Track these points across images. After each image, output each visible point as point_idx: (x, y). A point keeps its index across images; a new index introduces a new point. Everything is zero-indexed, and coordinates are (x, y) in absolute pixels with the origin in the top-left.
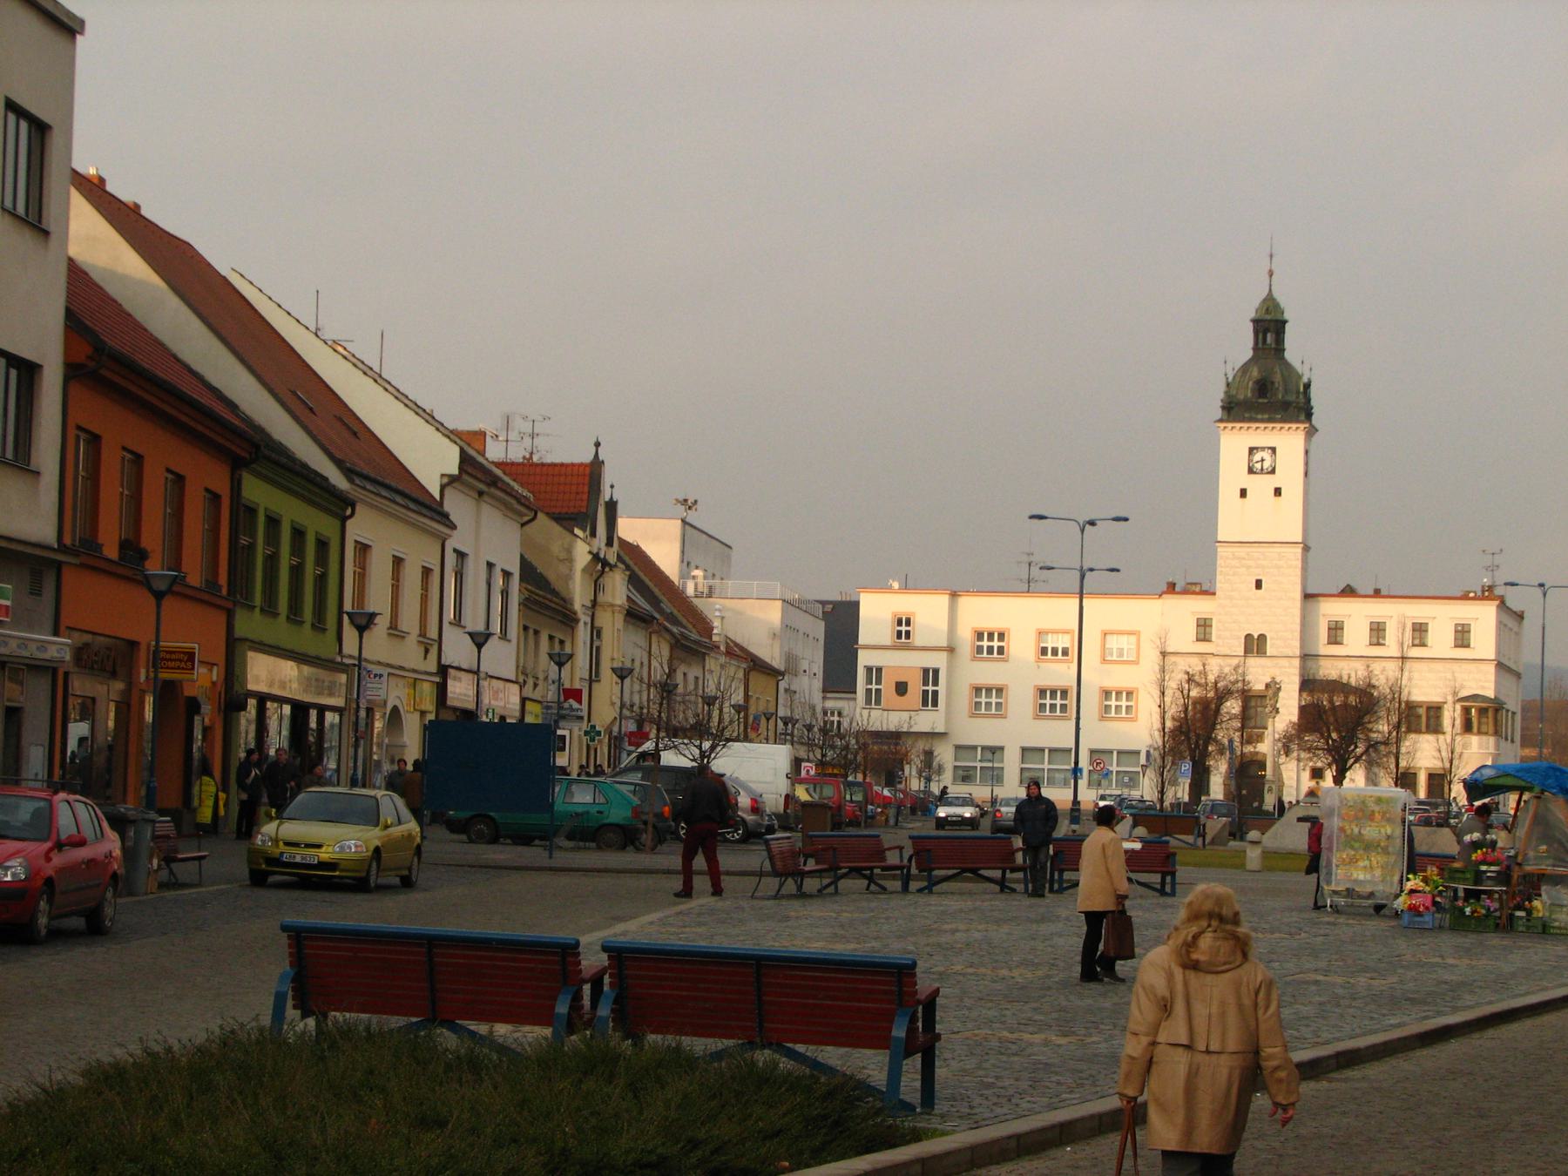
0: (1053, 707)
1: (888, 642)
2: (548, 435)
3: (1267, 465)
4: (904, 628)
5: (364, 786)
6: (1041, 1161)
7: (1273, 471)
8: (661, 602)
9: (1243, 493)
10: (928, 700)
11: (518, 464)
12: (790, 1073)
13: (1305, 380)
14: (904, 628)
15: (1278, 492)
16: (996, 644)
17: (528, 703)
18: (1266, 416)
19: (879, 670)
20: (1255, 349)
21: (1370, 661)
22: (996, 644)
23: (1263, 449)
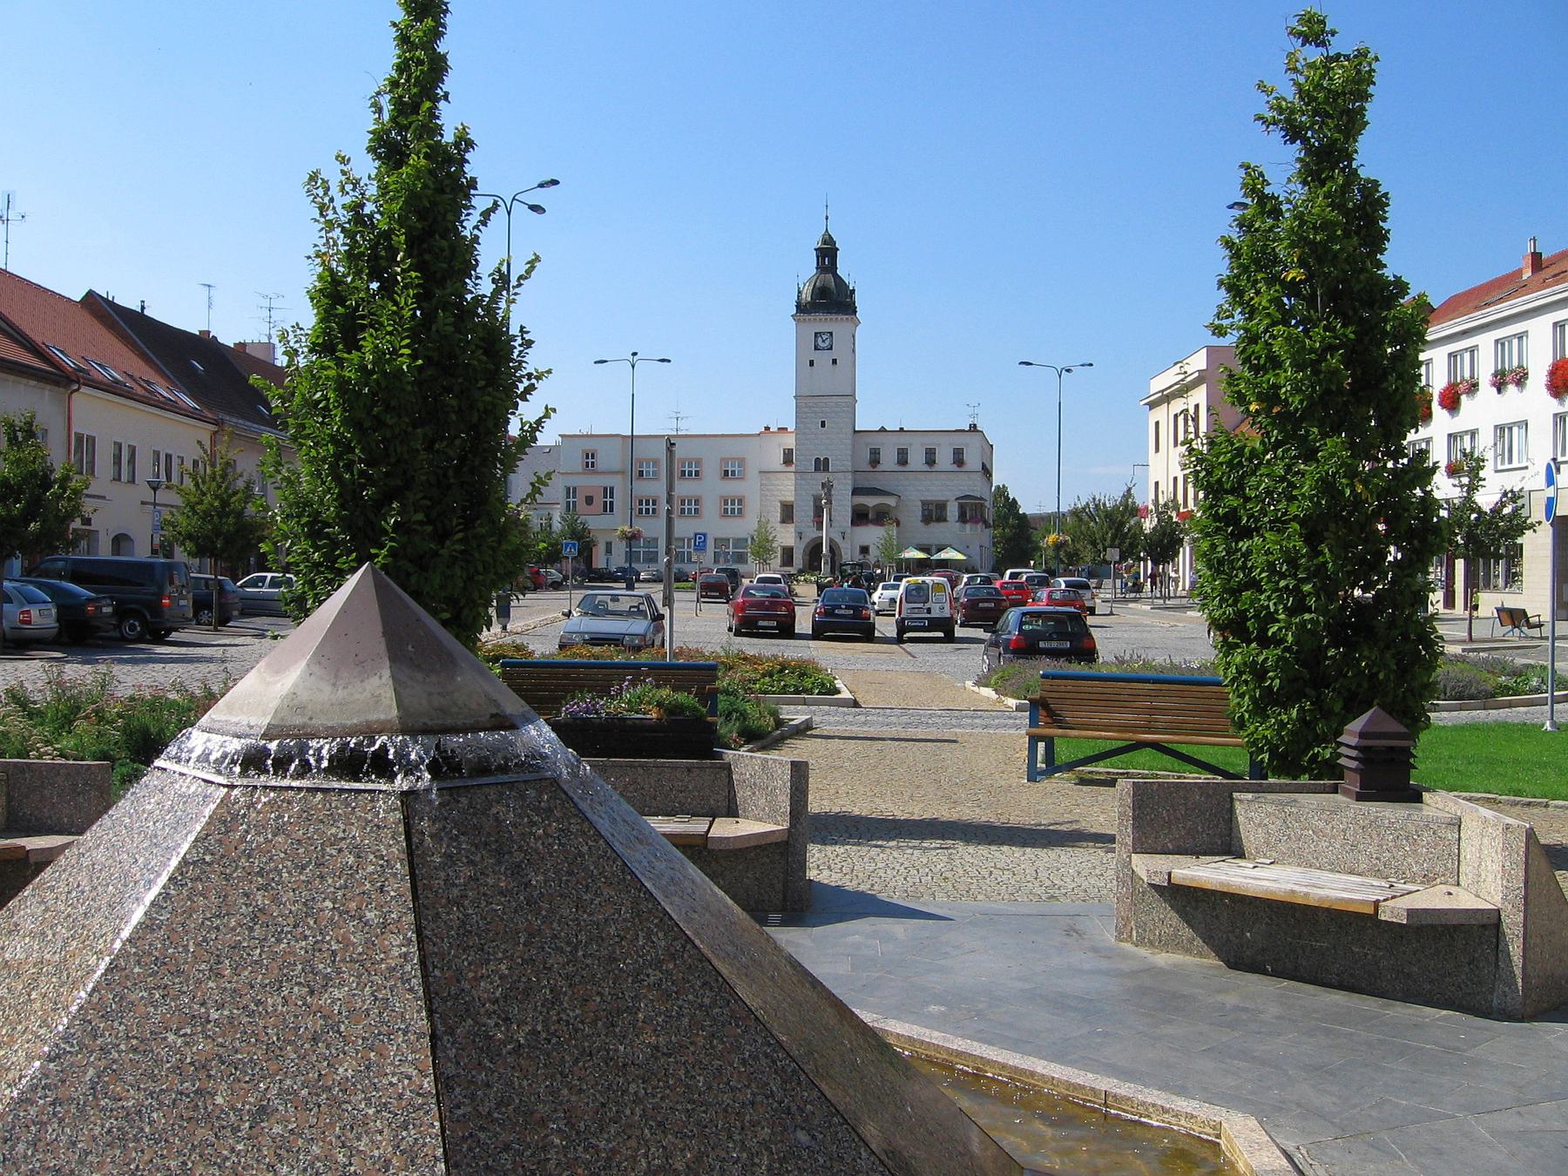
4: (590, 460)
9: (812, 363)
12: (536, 754)
14: (590, 460)
15: (834, 362)
17: (1467, 638)
19: (575, 489)
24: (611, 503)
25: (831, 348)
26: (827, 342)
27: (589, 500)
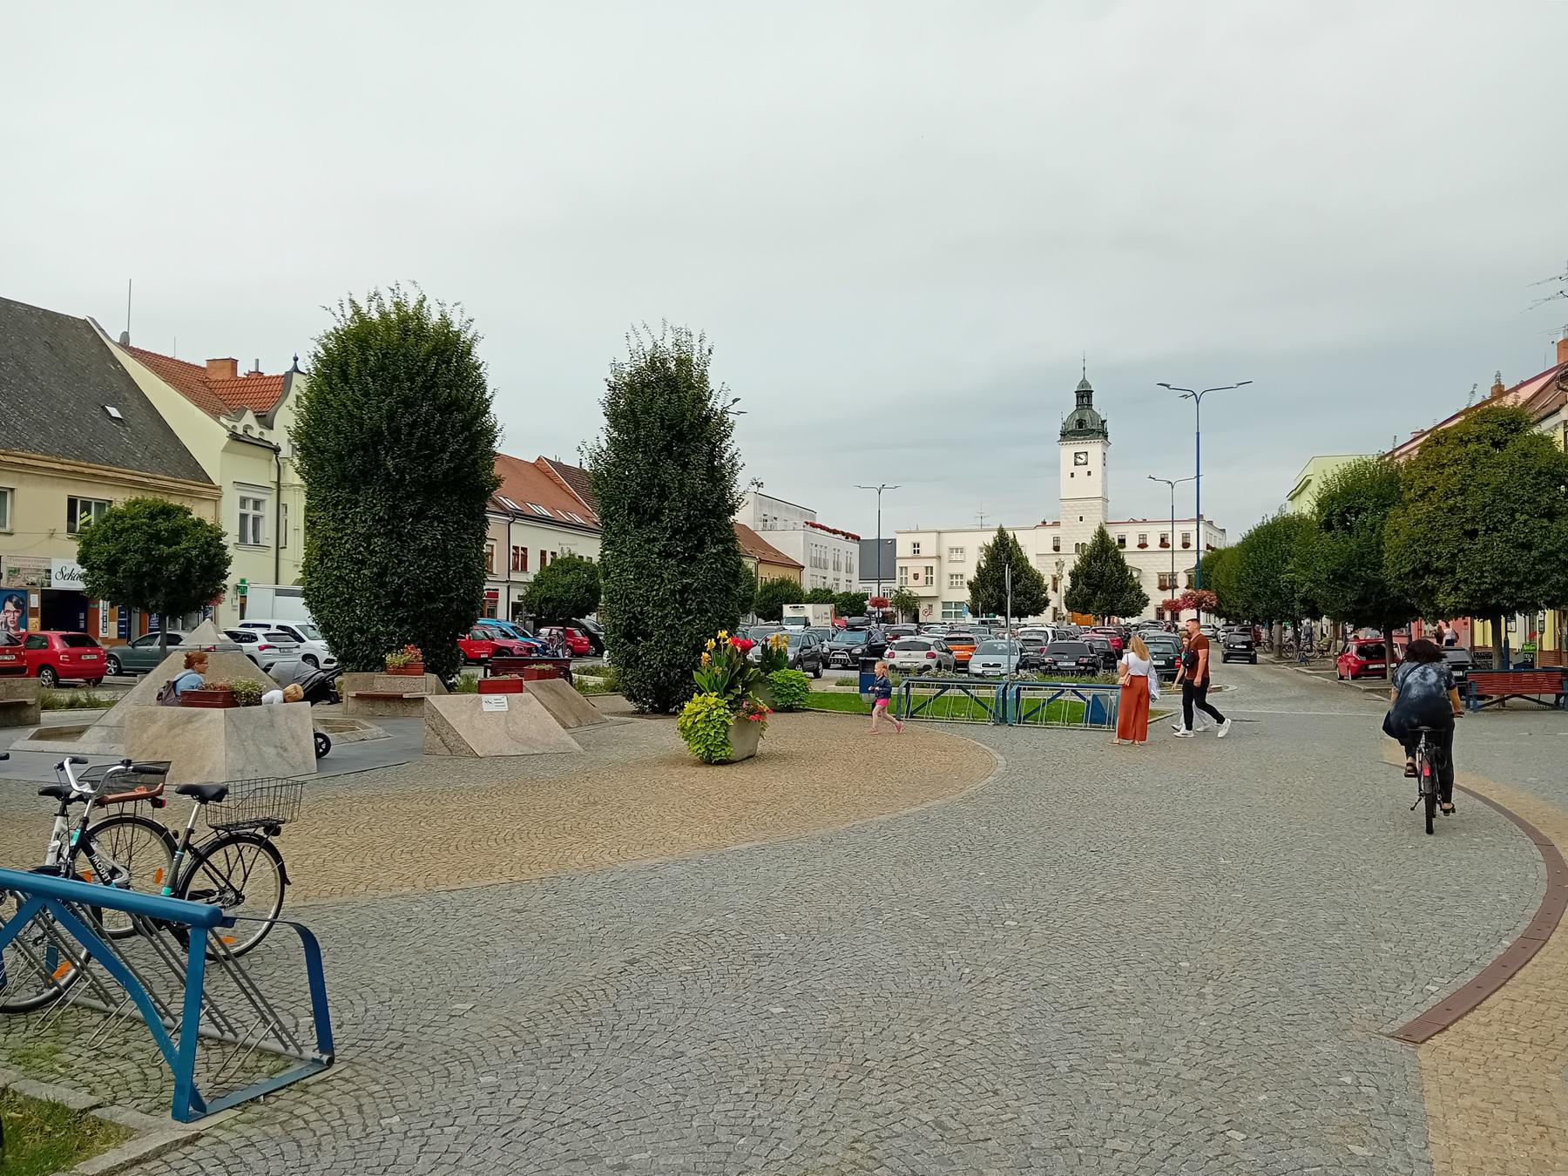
0: (957, 582)
1: (910, 556)
2: (1550, 280)
3: (1078, 460)
4: (916, 549)
5: (272, 618)
9: (1072, 475)
10: (929, 581)
14: (916, 549)
15: (1089, 473)
16: (959, 580)
22: (959, 580)
23: (1081, 453)
24: (932, 578)
25: (1086, 464)
26: (1081, 456)
27: (916, 577)
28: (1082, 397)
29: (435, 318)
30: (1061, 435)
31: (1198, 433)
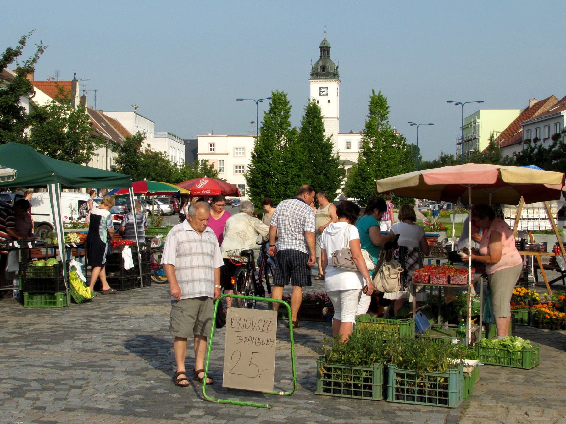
1: (207, 152)
4: (212, 148)
6: (520, 377)
7: (327, 95)
8: (119, 137)
11: (46, 82)
13: (336, 66)
14: (212, 148)
15: (329, 101)
16: (241, 169)
18: (325, 77)
20: (321, 56)
21: (521, 367)
22: (241, 169)
23: (324, 88)
28: (324, 50)
29: (322, 121)
30: (311, 75)
31: (257, 117)
